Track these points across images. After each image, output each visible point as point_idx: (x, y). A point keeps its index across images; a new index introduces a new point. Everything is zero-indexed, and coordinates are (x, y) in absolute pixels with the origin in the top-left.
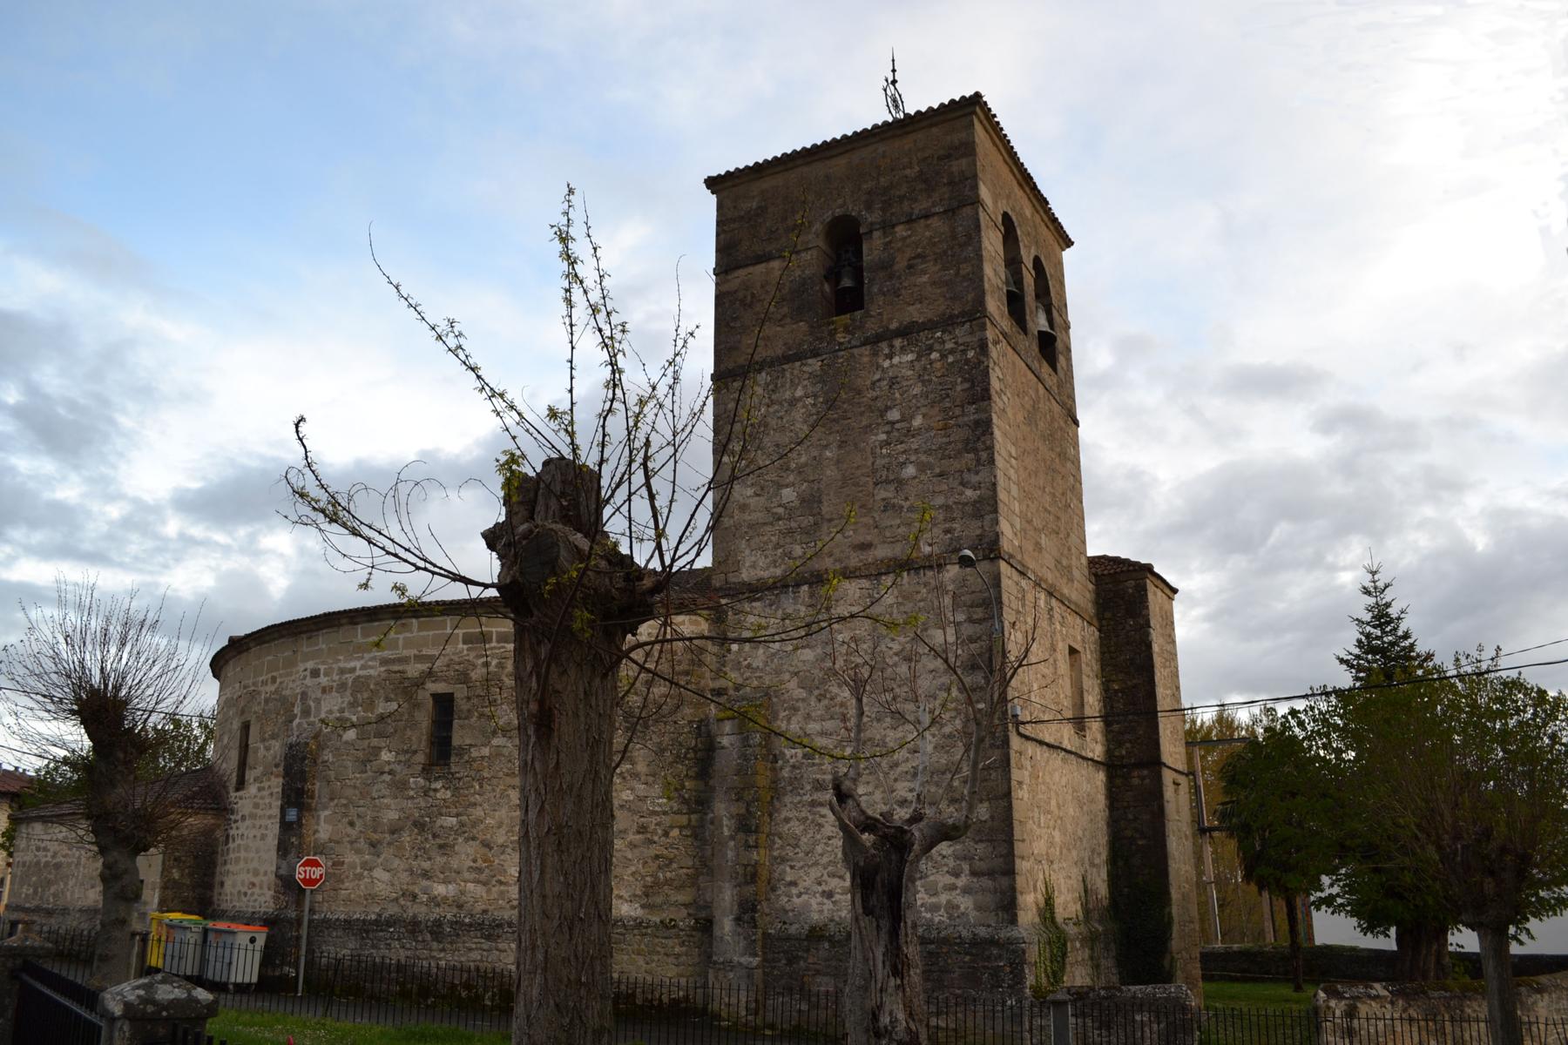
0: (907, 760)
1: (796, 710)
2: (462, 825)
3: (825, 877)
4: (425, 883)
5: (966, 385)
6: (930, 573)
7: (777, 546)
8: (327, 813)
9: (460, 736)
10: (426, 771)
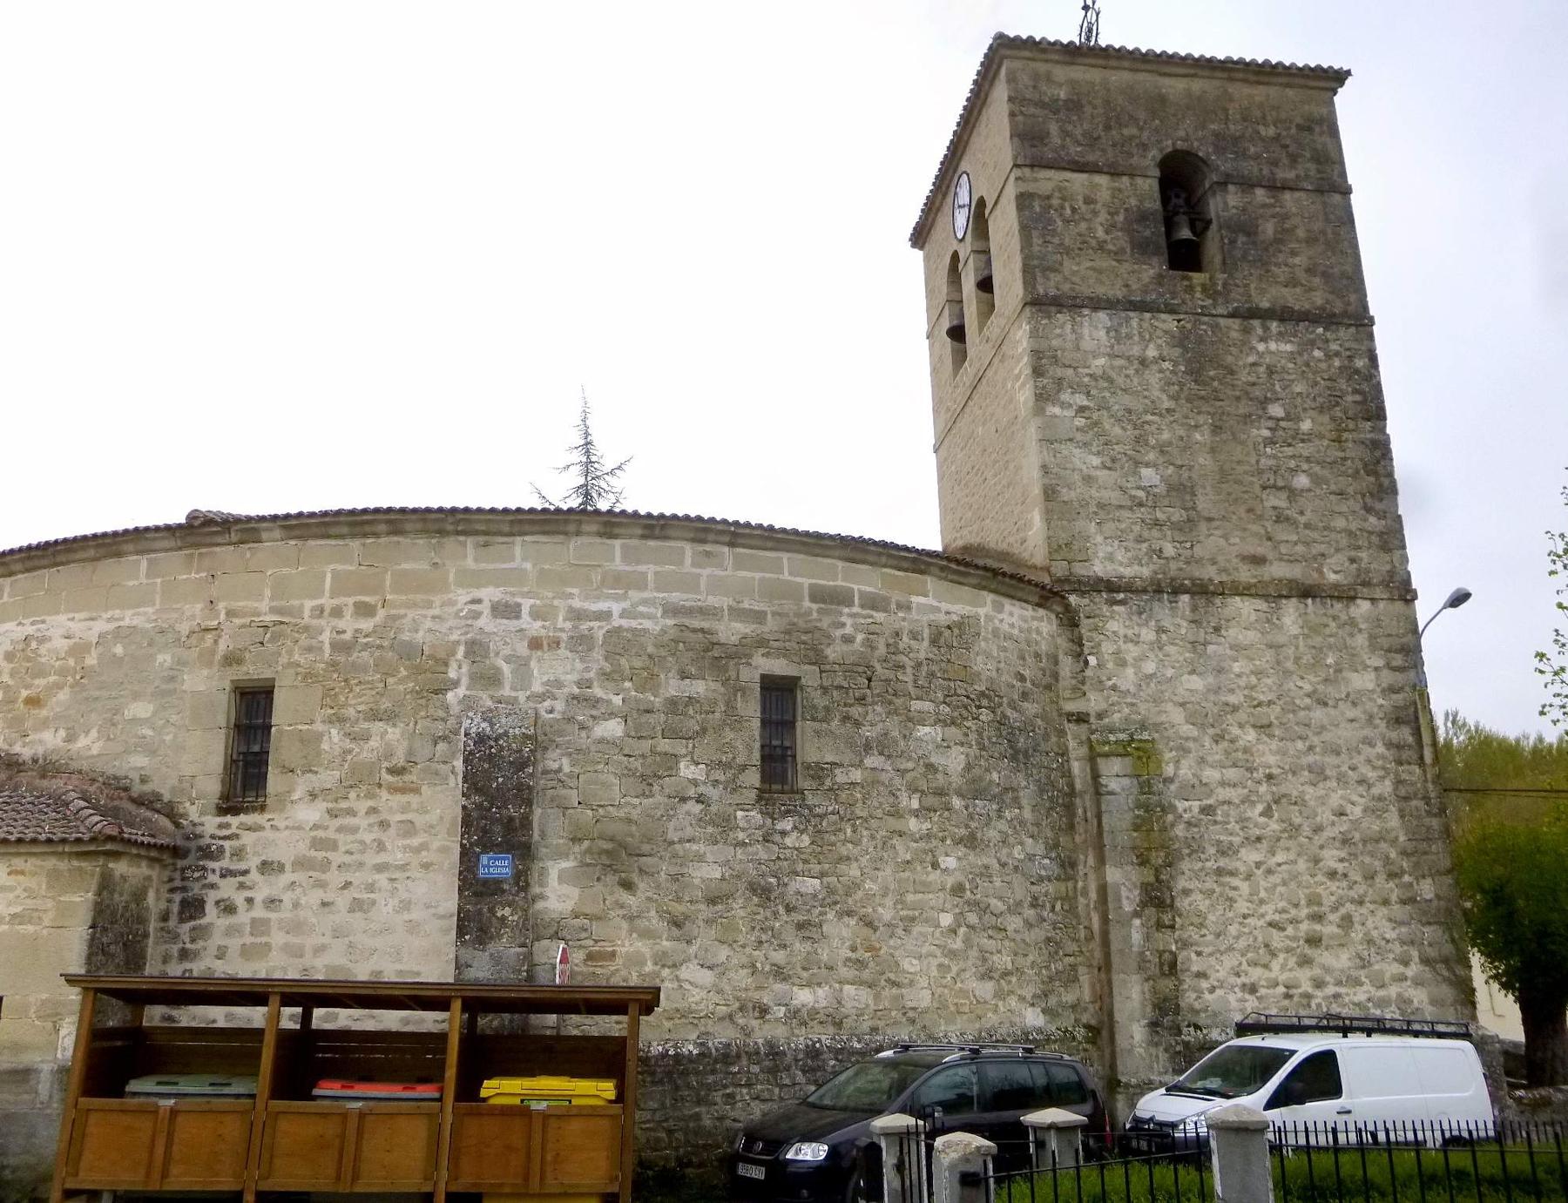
0: (1333, 824)
1: (1187, 751)
2: (831, 891)
3: (1245, 966)
4: (779, 987)
5: (1358, 398)
6: (1338, 606)
7: (1140, 540)
8: (565, 864)
9: (811, 746)
10: (764, 797)
